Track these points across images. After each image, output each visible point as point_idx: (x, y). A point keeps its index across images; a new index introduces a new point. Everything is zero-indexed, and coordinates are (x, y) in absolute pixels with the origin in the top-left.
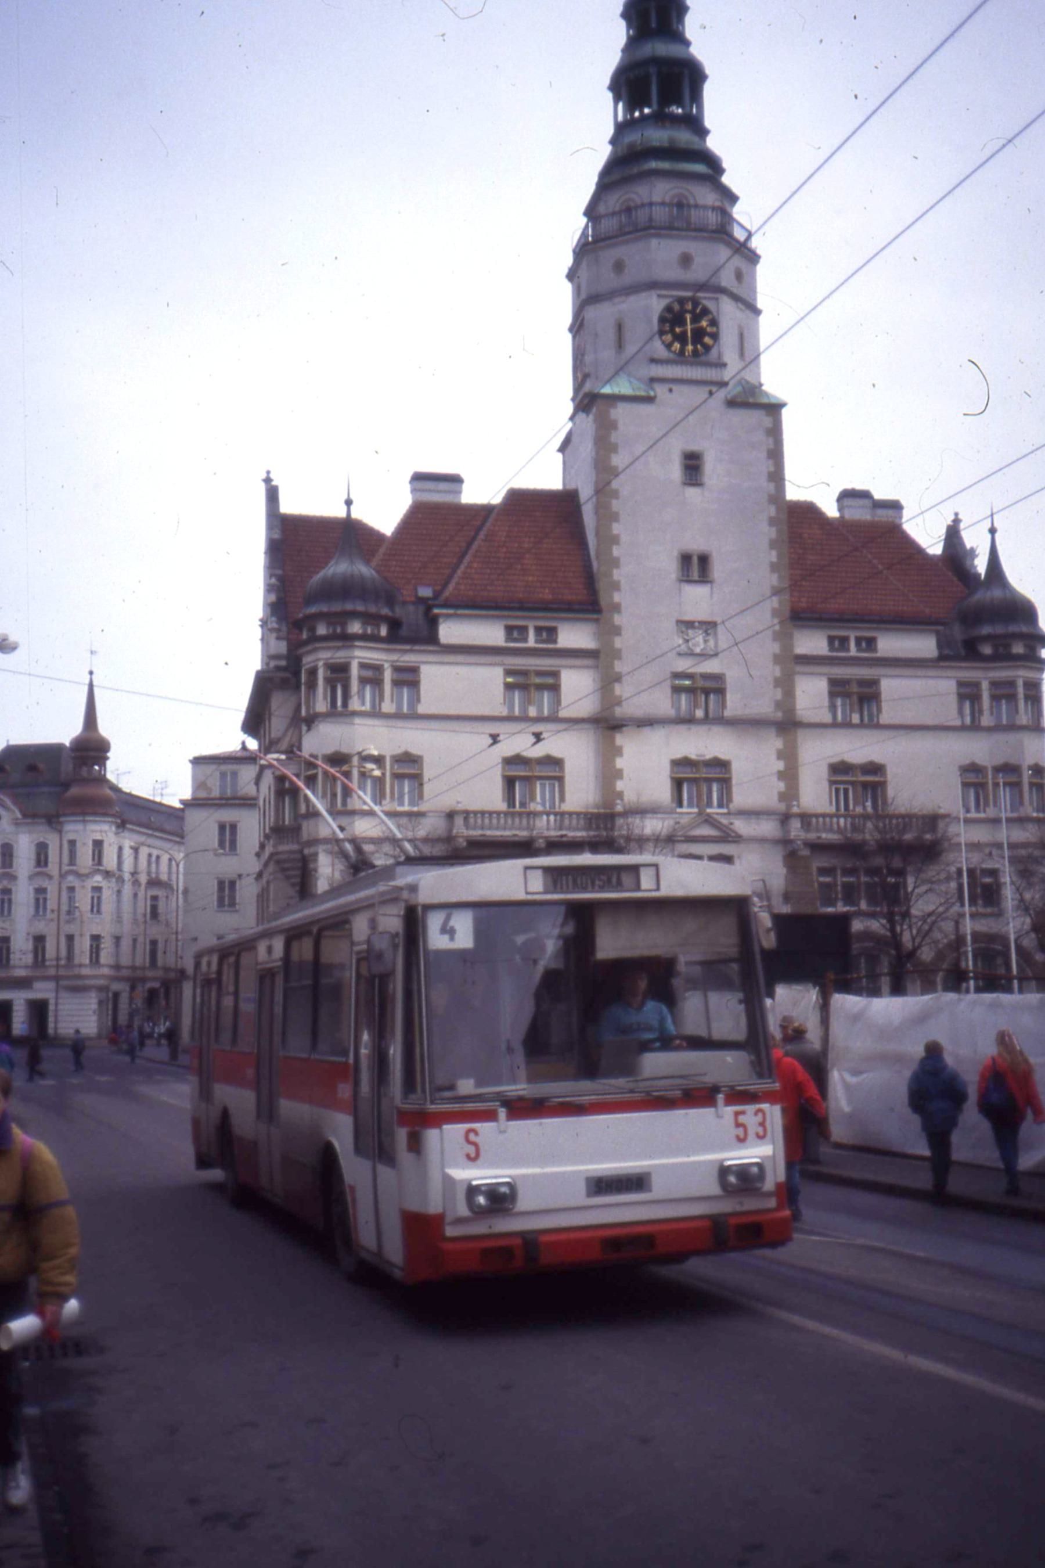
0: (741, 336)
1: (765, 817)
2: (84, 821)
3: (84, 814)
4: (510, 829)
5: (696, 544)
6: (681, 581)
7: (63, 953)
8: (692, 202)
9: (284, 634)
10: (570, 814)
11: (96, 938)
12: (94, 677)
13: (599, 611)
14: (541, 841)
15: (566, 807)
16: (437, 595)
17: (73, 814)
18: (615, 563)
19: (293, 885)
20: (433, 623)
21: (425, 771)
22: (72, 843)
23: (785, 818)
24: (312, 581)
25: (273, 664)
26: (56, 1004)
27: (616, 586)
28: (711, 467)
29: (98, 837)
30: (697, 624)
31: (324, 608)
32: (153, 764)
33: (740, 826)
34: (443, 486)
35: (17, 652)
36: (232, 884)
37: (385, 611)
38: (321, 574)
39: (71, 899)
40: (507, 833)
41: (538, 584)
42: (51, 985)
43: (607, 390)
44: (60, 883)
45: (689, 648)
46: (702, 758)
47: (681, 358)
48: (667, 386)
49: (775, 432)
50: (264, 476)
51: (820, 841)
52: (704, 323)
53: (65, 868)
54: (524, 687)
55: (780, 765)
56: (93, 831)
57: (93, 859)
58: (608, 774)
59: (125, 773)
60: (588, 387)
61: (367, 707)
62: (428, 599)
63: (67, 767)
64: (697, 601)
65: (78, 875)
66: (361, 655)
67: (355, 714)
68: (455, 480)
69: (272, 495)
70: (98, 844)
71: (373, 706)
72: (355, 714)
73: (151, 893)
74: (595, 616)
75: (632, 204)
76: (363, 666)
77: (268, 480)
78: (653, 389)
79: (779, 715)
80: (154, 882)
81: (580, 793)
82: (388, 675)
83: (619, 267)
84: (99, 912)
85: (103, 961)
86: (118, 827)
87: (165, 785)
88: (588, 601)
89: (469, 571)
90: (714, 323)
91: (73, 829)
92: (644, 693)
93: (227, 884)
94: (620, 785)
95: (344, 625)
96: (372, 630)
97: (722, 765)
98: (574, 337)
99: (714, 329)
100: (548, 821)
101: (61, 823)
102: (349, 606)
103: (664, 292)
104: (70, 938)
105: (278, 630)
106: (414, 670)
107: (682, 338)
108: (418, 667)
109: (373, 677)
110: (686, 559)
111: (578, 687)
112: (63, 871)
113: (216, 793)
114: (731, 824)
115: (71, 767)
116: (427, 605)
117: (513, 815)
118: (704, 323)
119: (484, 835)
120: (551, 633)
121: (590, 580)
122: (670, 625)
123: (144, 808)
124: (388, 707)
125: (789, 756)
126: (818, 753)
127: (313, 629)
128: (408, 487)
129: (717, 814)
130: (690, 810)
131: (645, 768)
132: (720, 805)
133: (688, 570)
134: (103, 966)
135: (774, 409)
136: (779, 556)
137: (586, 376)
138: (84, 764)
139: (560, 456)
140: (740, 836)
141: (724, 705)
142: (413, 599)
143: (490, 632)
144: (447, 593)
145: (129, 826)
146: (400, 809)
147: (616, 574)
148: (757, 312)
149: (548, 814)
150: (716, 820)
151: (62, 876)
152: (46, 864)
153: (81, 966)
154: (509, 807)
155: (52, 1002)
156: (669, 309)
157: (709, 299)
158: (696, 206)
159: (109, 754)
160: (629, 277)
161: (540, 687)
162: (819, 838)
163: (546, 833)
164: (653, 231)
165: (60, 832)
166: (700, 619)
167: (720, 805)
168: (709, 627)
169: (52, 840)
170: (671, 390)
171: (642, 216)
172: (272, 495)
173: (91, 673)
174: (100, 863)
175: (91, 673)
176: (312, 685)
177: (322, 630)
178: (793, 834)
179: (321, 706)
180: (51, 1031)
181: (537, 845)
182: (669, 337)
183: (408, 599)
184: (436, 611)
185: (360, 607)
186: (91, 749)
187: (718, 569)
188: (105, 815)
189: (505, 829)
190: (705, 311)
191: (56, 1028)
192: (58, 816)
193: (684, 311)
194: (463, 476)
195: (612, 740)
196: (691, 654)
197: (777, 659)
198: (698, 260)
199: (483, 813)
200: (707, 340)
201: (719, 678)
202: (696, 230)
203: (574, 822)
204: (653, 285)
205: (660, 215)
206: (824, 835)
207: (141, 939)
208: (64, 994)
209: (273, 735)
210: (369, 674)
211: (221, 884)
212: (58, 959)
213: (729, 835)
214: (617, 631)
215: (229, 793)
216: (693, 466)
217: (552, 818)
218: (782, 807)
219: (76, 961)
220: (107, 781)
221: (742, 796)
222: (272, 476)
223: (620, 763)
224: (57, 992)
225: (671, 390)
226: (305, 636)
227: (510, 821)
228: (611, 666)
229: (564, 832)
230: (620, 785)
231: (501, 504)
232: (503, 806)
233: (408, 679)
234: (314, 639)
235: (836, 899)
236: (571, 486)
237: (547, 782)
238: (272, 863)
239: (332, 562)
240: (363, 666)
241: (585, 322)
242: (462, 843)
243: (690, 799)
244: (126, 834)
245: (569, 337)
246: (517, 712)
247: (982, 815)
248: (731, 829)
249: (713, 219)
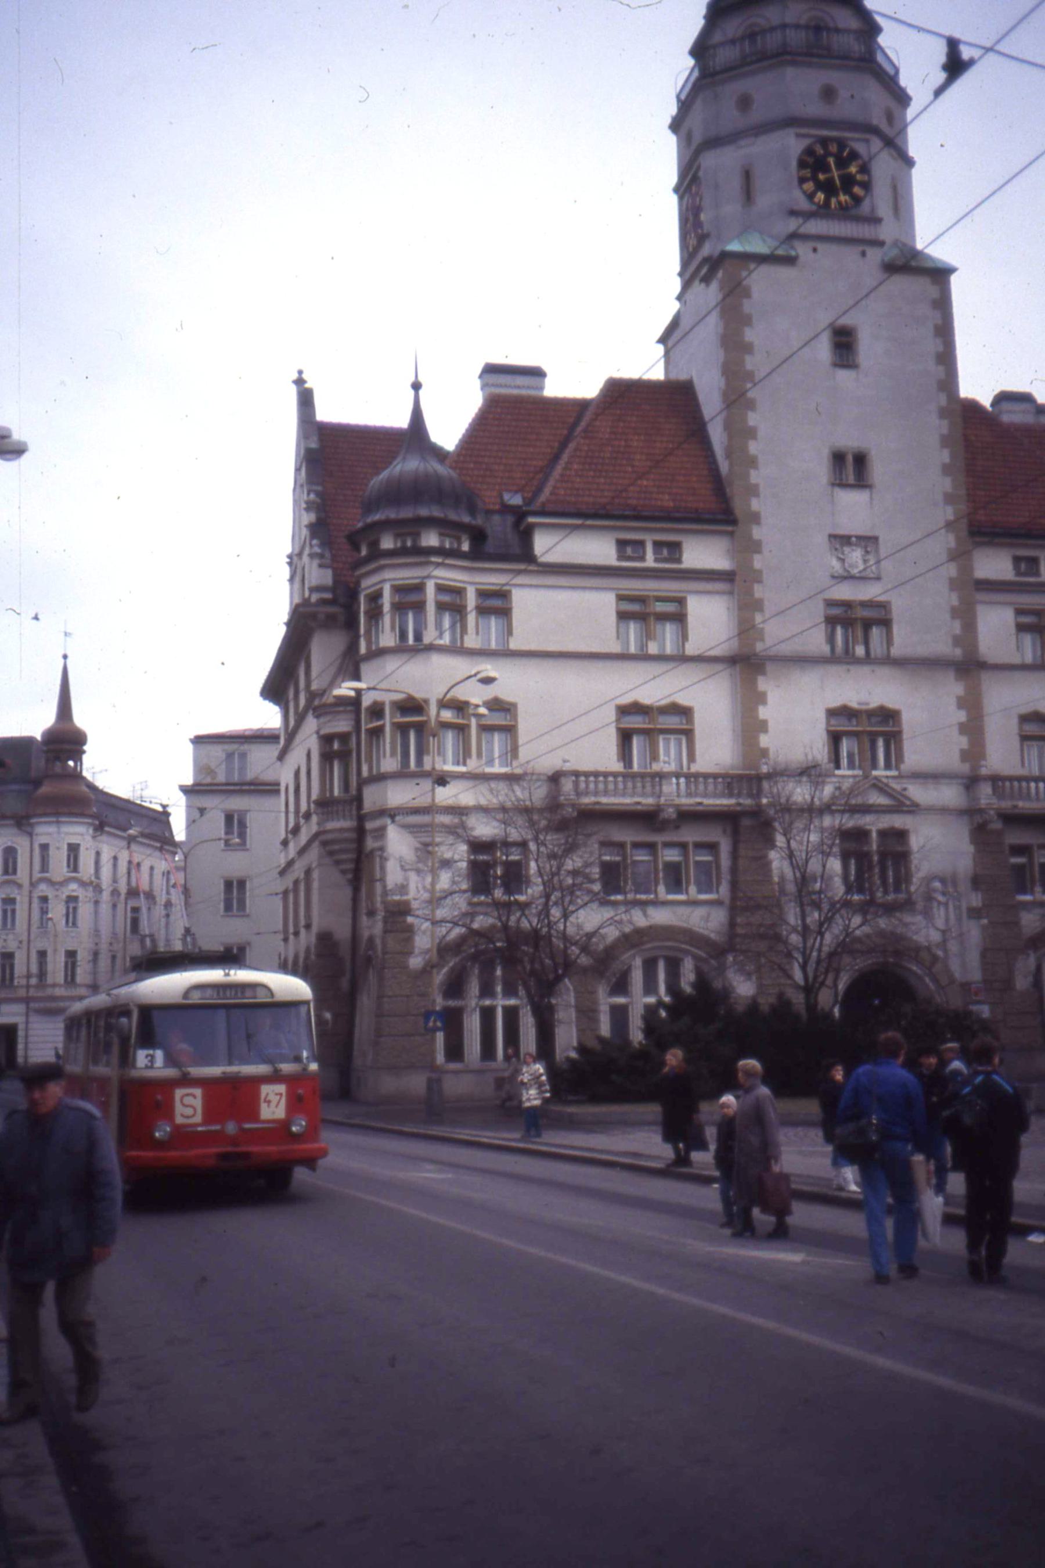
0: (895, 188)
1: (947, 781)
2: (58, 822)
3: (57, 814)
4: (632, 795)
5: (850, 441)
6: (833, 485)
7: (34, 969)
8: (831, 25)
9: (328, 561)
10: (706, 776)
11: (71, 954)
12: (68, 661)
13: (734, 522)
14: (671, 810)
15: (695, 768)
16: (528, 502)
17: (45, 815)
18: (752, 462)
19: (344, 872)
20: (526, 536)
21: (520, 720)
22: (45, 847)
23: (971, 782)
24: (372, 482)
25: (314, 598)
26: (27, 1029)
27: (753, 491)
28: (869, 347)
29: (74, 840)
30: (854, 539)
31: (392, 514)
32: (139, 759)
33: (917, 793)
34: (520, 380)
35: (25, 457)
36: (242, 883)
37: (466, 519)
38: (384, 475)
39: (44, 912)
40: (628, 800)
41: (655, 490)
42: (20, 1008)
43: (734, 247)
44: (30, 892)
45: (845, 570)
46: (864, 707)
47: (823, 211)
48: (811, 244)
49: (943, 304)
50: (295, 376)
51: (1017, 811)
52: (853, 169)
53: (37, 875)
54: (641, 617)
55: (962, 716)
56: (67, 834)
57: (68, 866)
58: (750, 728)
59: (101, 772)
60: (706, 250)
61: (446, 640)
62: (520, 507)
63: (38, 764)
64: (854, 509)
65: (50, 882)
66: (441, 574)
67: (431, 648)
68: (537, 373)
69: (306, 399)
70: (74, 850)
71: (453, 639)
72: (431, 648)
73: (132, 903)
74: (730, 528)
75: (757, 29)
76: (440, 589)
77: (300, 382)
78: (792, 248)
79: (958, 652)
80: (133, 893)
81: (716, 749)
82: (471, 600)
83: (745, 103)
84: (74, 924)
85: (79, 979)
86: (96, 829)
87: (145, 785)
88: (719, 509)
89: (568, 472)
90: (864, 169)
91: (46, 831)
92: (792, 623)
93: (235, 883)
94: (764, 741)
95: (416, 536)
96: (451, 543)
97: (888, 716)
98: (681, 198)
99: (866, 178)
100: (678, 784)
101: (32, 825)
102: (423, 512)
103: (804, 131)
104: (42, 954)
105: (321, 556)
106: (503, 595)
107: (829, 188)
108: (510, 592)
109: (452, 603)
110: (838, 458)
111: (709, 619)
112: (34, 880)
113: (221, 778)
114: (905, 789)
115: (42, 763)
116: (519, 515)
117: (634, 776)
118: (853, 169)
119: (598, 803)
120: (674, 549)
121: (719, 485)
122: (820, 539)
123: (123, 810)
124: (471, 641)
125: (972, 704)
126: (1007, 700)
127: (374, 544)
128: (478, 383)
129: (887, 777)
130: (850, 773)
131: (796, 718)
132: (888, 766)
133: (841, 473)
134: (80, 986)
135: (940, 274)
136: (953, 456)
137: (702, 238)
138: (57, 758)
139: (661, 348)
140: (917, 805)
141: (889, 641)
142: (497, 507)
143: (597, 548)
144: (543, 497)
145: (107, 829)
146: (488, 770)
147: (755, 477)
148: (909, 163)
149: (677, 775)
150: (887, 785)
151: (33, 885)
152: (15, 872)
153: (54, 985)
154: (625, 767)
155: (21, 1027)
156: (809, 151)
157: (858, 140)
158: (837, 30)
159: (85, 748)
160: (758, 114)
161: (663, 617)
162: (1015, 807)
163: (677, 801)
164: (789, 57)
165: (31, 835)
166: (860, 533)
167: (888, 766)
168: (868, 542)
169: (22, 844)
170: (815, 250)
171: (773, 41)
172: (306, 399)
173: (65, 657)
174: (75, 869)
175: (65, 657)
176: (375, 614)
177: (387, 543)
178: (983, 802)
179: (387, 639)
180: (20, 1060)
181: (664, 815)
182: (809, 186)
183: (491, 507)
184: (531, 520)
185: (436, 512)
186: (65, 741)
187: (878, 470)
188: (82, 815)
189: (624, 795)
190: (854, 156)
191: (26, 1057)
192: (28, 817)
193: (828, 154)
194: (545, 368)
195: (753, 683)
196: (848, 577)
197: (954, 584)
198: (843, 94)
199: (596, 774)
200: (857, 190)
201: (884, 606)
202: (838, 57)
203: (711, 788)
204: (791, 122)
205: (796, 38)
206: (1021, 804)
207: (119, 955)
208: (33, 1018)
209: (314, 687)
210: (446, 598)
211: (228, 885)
212: (29, 976)
213: (902, 804)
214: (756, 547)
215: (236, 778)
216: (844, 343)
217: (682, 780)
218: (965, 768)
219: (50, 980)
220: (84, 778)
221: (917, 753)
222: (304, 376)
223: (763, 713)
224: (27, 1015)
225: (815, 250)
226: (364, 552)
227: (630, 785)
228: (750, 592)
229: (698, 800)
230: (764, 741)
231: (599, 396)
232: (618, 767)
233: (496, 605)
234: (376, 553)
235: (1033, 883)
236: (681, 375)
237: (672, 737)
238: (316, 844)
239: (399, 459)
240: (440, 589)
241: (701, 174)
242: (569, 812)
243: (850, 756)
244: (104, 838)
245: (675, 198)
246: (632, 650)
247: (462, 769)
248: (903, 795)
249: (857, 48)
